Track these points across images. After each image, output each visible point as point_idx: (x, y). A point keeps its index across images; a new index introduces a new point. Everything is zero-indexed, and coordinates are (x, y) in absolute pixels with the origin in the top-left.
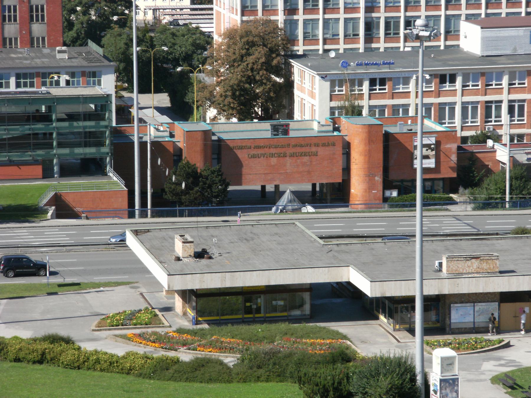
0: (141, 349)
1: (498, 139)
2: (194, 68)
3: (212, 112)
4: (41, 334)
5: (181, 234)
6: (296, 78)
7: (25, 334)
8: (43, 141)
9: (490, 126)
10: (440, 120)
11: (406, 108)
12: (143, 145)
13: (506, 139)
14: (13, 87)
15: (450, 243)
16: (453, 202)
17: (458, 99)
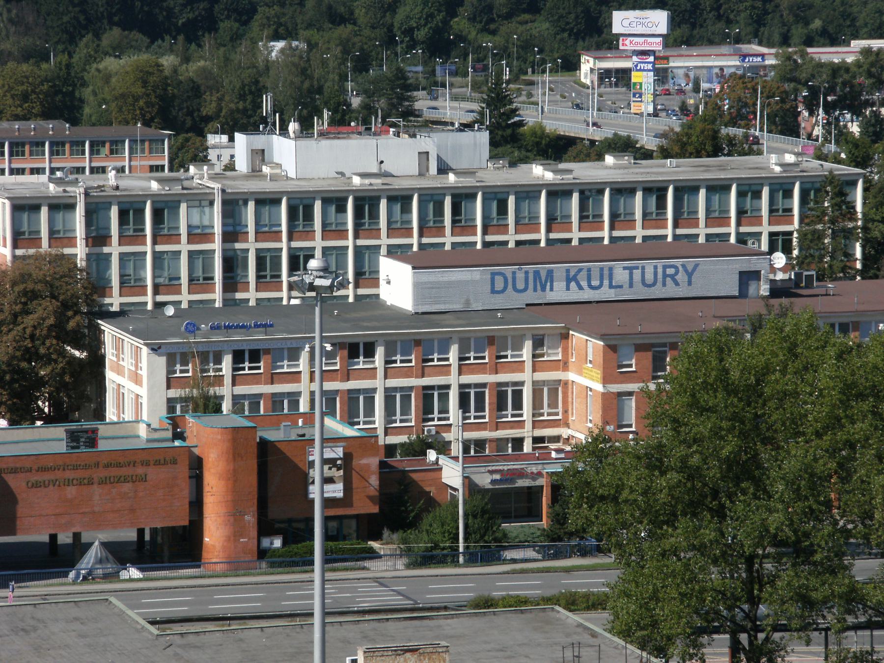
1: (443, 448)
6: (109, 351)
9: (431, 427)
10: (350, 419)
11: (293, 399)
13: (456, 449)
15: (369, 626)
16: (373, 555)
17: (379, 383)
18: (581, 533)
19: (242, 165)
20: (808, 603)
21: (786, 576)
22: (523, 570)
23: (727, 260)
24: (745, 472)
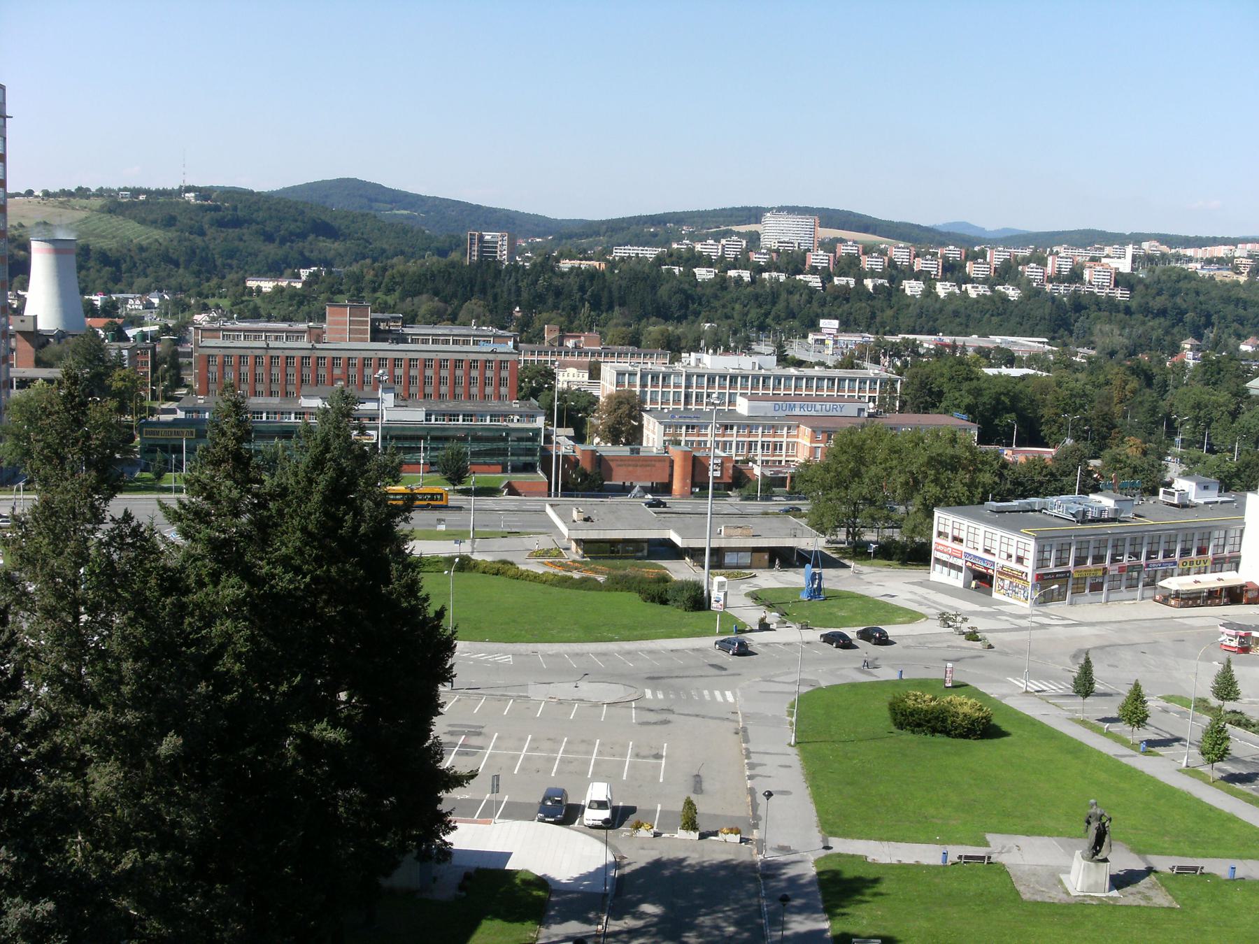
0: (551, 570)
1: (755, 462)
2: (588, 415)
3: (597, 440)
4: (497, 559)
5: (577, 507)
6: (645, 422)
7: (489, 558)
8: (503, 453)
9: (751, 455)
10: (724, 450)
11: (705, 442)
12: (558, 456)
13: (759, 463)
14: (488, 422)
15: (726, 519)
16: (729, 496)
17: (734, 439)
18: (799, 493)
19: (693, 364)
20: (874, 519)
21: (867, 510)
22: (779, 503)
23: (855, 403)
24: (856, 474)
